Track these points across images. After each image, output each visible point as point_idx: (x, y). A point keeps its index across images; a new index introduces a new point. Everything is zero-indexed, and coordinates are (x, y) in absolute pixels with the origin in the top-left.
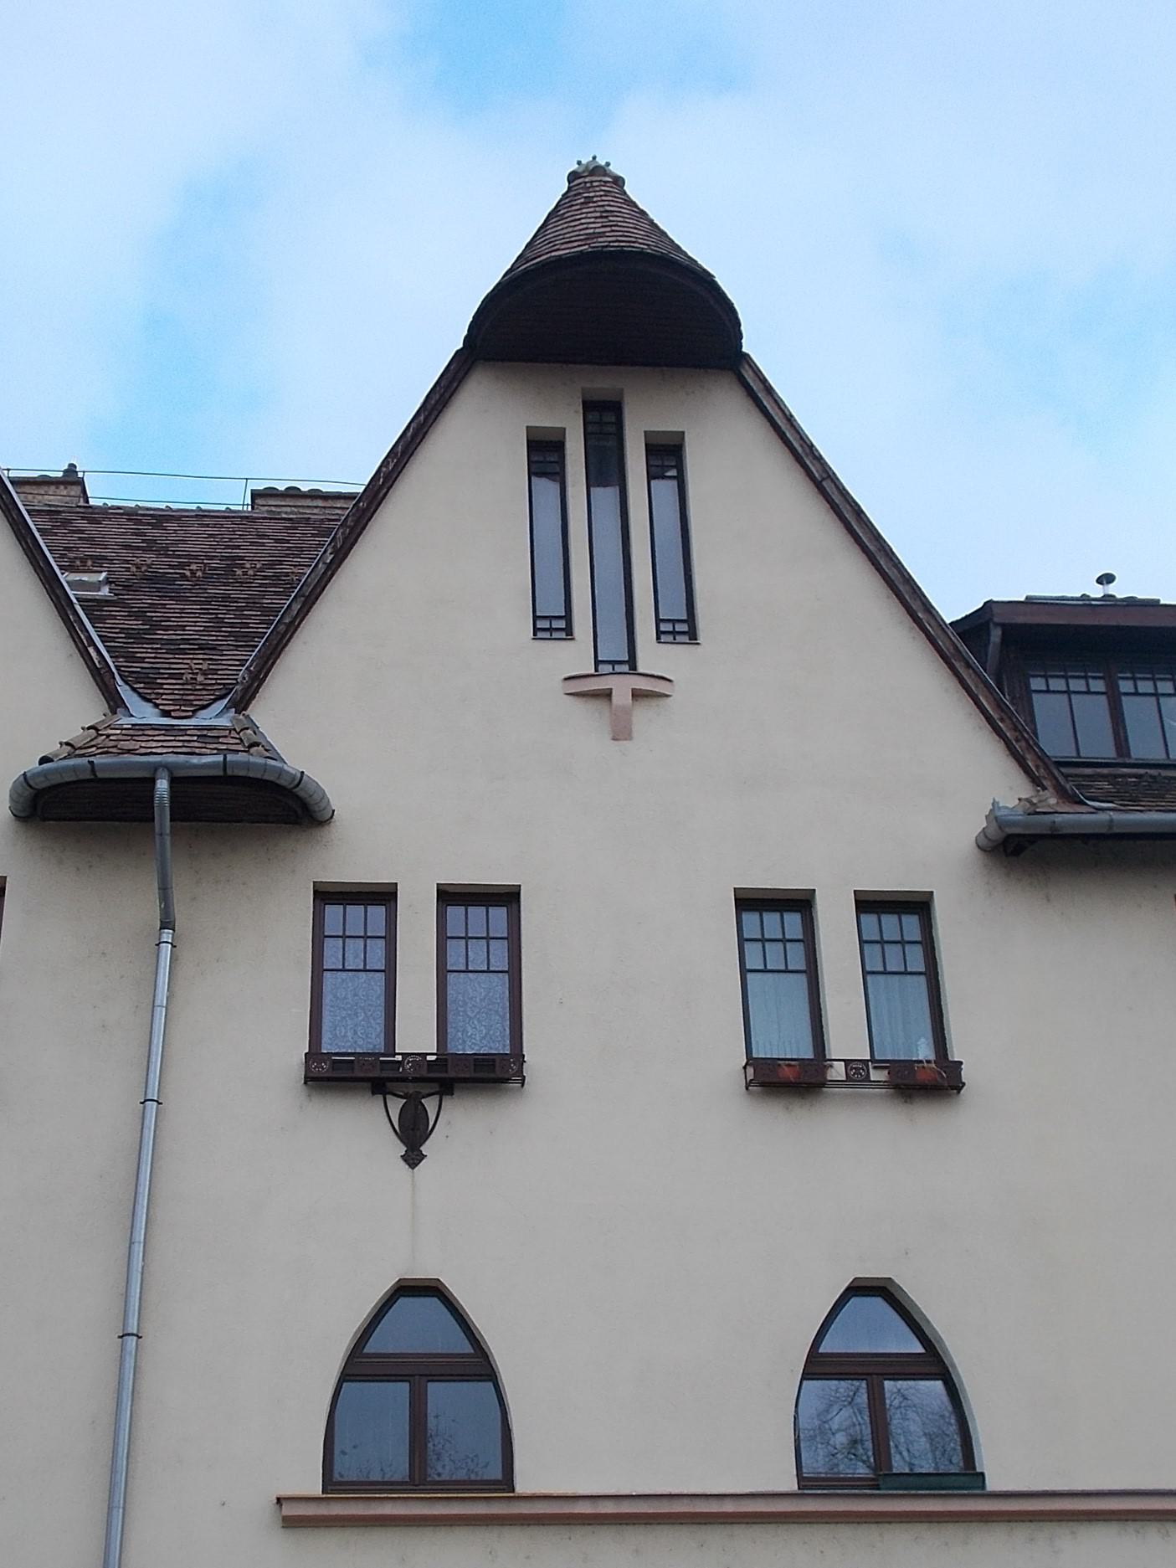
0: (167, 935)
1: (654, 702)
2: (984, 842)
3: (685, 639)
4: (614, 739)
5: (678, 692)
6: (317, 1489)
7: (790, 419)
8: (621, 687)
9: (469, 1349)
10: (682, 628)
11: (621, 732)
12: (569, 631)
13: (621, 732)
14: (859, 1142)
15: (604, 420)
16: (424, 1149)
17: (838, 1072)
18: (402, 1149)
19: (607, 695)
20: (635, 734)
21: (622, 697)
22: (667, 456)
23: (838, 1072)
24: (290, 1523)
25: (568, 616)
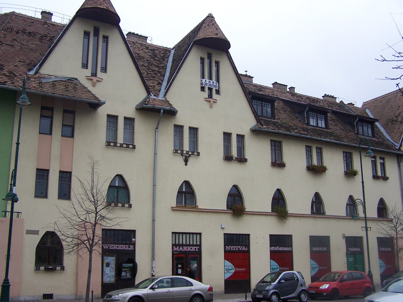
0: (157, 130)
1: (215, 103)
2: (251, 129)
3: (104, 71)
4: (210, 108)
5: (218, 102)
6: (310, 213)
7: (233, 62)
8: (95, 79)
9: (237, 193)
10: (104, 70)
11: (211, 107)
12: (87, 68)
13: (211, 107)
14: (235, 167)
15: (210, 57)
16: (187, 163)
17: (118, 145)
18: (185, 163)
19: (210, 101)
20: (213, 108)
21: (212, 102)
22: (106, 38)
23: (118, 145)
24: (173, 210)
25: (87, 64)
